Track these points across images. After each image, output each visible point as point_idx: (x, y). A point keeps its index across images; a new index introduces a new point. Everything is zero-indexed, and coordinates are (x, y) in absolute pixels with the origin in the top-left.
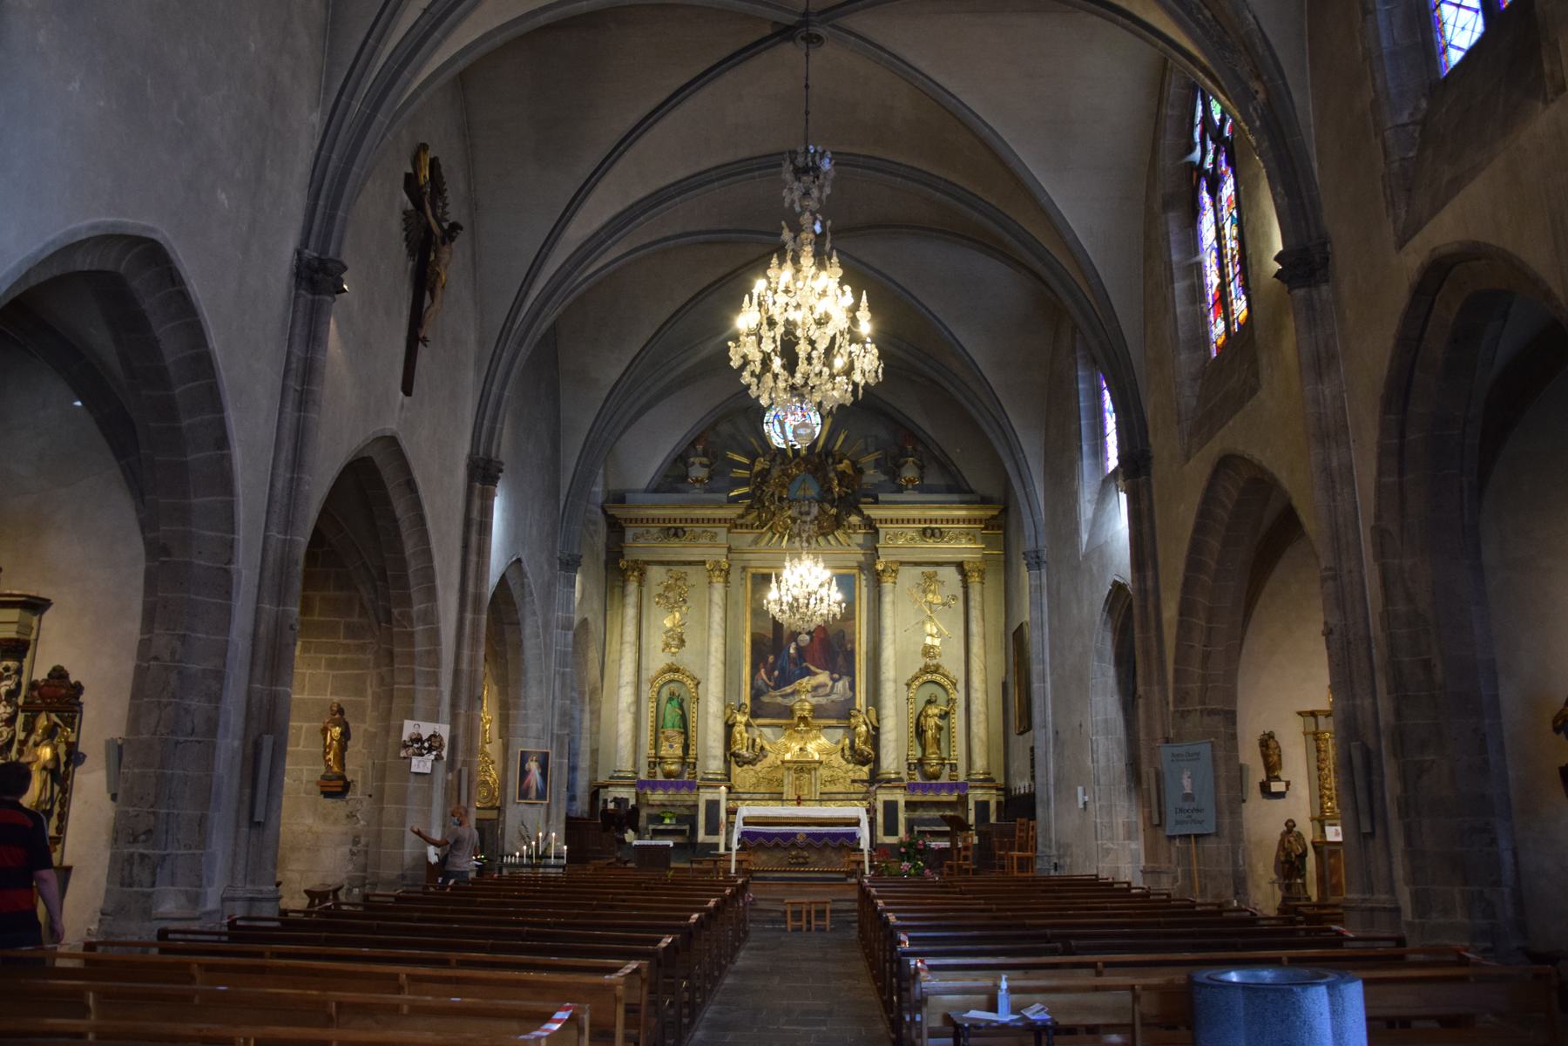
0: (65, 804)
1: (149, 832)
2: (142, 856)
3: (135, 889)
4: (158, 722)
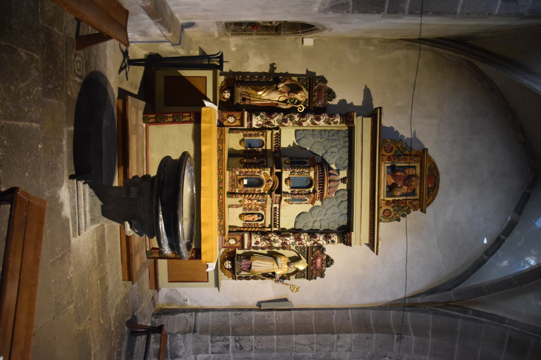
0: (255, 278)
1: (241, 348)
2: (227, 346)
3: (210, 344)
4: (302, 345)
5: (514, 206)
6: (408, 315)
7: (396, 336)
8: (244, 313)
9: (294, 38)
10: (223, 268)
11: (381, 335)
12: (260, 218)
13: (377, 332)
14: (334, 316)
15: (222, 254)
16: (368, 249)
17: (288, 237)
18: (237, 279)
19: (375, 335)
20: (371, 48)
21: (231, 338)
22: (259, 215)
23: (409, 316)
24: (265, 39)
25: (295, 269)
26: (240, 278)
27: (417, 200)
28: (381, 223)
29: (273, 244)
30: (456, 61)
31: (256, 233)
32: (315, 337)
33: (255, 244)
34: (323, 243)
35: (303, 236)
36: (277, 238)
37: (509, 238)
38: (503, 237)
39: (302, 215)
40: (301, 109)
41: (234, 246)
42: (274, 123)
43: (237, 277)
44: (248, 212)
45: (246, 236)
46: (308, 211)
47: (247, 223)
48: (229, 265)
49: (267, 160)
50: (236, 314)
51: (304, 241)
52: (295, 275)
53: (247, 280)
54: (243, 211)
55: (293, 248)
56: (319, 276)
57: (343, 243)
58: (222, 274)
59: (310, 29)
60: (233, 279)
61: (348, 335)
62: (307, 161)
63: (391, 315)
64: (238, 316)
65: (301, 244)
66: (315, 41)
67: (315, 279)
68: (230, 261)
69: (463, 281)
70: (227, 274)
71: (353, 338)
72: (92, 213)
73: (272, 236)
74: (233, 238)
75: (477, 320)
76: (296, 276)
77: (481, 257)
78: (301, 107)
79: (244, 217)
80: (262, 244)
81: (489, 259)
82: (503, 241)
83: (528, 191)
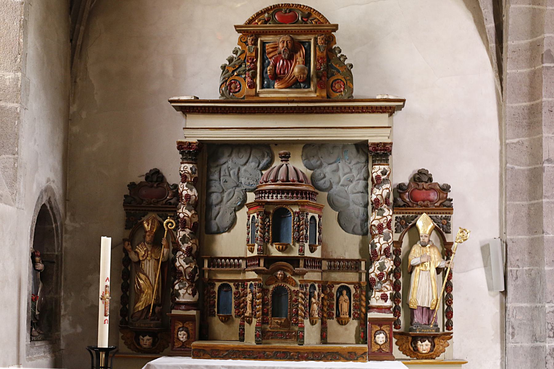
6: (513, 44)
7: (546, 65)
8: (511, 319)
10: (431, 355)
11: (544, 89)
12: (345, 292)
13: (540, 96)
14: (516, 167)
15: (407, 356)
16: (398, 115)
17: (376, 246)
18: (451, 331)
19: (544, 99)
20: (84, 115)
21: (550, 345)
22: (340, 291)
23: (516, 42)
24: (65, 279)
25: (434, 233)
26: (449, 325)
27: (316, 39)
29: (386, 270)
31: (368, 298)
32: (548, 200)
33: (386, 301)
34: (387, 189)
35: (374, 221)
36: (377, 264)
39: (342, 222)
40: (170, 224)
41: (388, 335)
44: (334, 312)
45: (371, 315)
47: (352, 312)
49: (249, 280)
50: (513, 335)
52: (444, 233)
53: (452, 315)
55: (396, 237)
56: (447, 194)
57: (388, 156)
58: (442, 355)
59: (50, 211)
61: (544, 144)
62: (251, 216)
63: (514, 71)
64: (516, 332)
68: (417, 342)
70: (441, 348)
71: (551, 135)
73: (373, 272)
74: (375, 337)
76: (447, 232)
78: (168, 223)
79: (341, 318)
80: (387, 289)
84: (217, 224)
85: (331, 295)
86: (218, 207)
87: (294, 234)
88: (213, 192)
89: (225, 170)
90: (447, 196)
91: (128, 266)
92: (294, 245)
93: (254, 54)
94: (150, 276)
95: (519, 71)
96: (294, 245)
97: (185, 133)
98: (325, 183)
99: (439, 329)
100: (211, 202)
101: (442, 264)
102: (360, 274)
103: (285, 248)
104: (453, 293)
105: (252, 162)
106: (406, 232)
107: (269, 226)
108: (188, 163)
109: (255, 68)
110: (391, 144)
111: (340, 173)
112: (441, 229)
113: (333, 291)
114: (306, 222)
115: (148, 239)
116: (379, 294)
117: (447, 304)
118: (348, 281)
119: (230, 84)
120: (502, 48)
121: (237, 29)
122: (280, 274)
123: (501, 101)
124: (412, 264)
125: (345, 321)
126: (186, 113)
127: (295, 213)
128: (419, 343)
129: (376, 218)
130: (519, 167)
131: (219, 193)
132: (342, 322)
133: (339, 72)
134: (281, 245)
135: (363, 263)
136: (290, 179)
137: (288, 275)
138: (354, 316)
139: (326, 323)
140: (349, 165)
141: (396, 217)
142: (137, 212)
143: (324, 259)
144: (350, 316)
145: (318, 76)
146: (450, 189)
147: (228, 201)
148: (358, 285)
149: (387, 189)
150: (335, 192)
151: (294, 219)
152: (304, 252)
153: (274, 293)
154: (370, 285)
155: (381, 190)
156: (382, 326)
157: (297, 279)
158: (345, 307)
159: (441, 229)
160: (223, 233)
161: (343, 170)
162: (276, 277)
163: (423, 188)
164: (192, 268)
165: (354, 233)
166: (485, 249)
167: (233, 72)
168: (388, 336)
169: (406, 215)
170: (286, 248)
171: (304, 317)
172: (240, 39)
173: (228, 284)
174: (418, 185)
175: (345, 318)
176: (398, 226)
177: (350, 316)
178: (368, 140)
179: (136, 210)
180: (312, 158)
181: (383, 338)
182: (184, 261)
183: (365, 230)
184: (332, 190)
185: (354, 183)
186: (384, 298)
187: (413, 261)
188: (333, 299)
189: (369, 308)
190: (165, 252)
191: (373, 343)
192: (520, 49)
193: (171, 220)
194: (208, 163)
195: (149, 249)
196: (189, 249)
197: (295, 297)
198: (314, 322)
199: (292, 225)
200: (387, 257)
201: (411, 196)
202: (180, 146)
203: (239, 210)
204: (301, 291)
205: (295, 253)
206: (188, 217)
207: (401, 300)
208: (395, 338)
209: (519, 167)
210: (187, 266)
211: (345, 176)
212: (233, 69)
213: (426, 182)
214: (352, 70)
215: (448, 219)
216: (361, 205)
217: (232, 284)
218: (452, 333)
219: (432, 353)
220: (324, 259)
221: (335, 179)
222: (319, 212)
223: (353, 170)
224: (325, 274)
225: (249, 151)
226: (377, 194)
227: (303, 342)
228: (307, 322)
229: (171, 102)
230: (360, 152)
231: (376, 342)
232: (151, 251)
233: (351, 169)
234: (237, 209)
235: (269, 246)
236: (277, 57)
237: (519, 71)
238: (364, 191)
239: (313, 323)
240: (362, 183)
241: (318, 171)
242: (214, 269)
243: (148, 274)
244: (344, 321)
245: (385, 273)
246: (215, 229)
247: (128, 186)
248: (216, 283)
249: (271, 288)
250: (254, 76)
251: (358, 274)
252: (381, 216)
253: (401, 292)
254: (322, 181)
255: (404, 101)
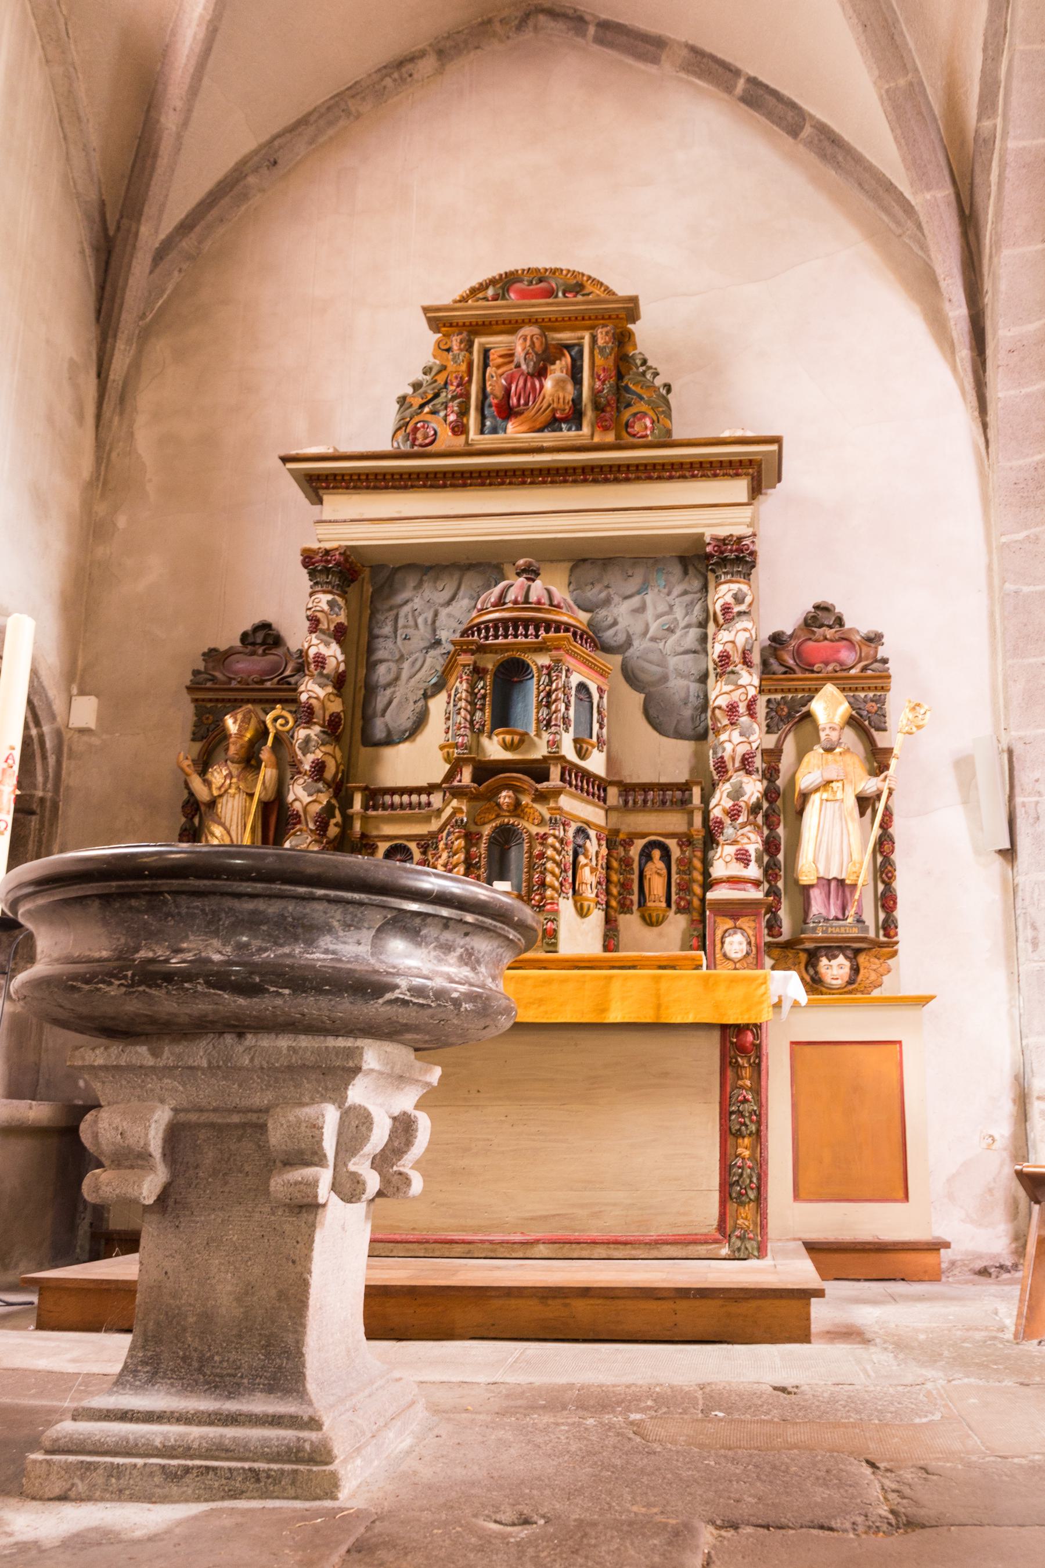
5: (641, 66)
6: (1009, 334)
9: (69, 758)
12: (656, 853)
14: (1026, 589)
17: (724, 750)
18: (895, 939)
20: (122, 521)
22: (646, 855)
23: (1015, 331)
26: (889, 926)
28: (677, 435)
29: (745, 798)
30: (180, 271)
31: (707, 863)
33: (747, 865)
34: (745, 630)
36: (725, 788)
37: (739, 65)
38: (741, 83)
39: (653, 712)
40: (280, 721)
42: (320, 803)
43: (885, 939)
44: (635, 898)
46: (643, 696)
47: (674, 897)
48: (834, 962)
51: (736, 696)
52: (873, 730)
53: (895, 903)
54: (632, 913)
56: (876, 648)
60: (895, 954)
63: (1012, 392)
65: (751, 706)
66: (82, 693)
67: (885, 661)
69: (890, 187)
70: (873, 976)
72: (239, 1385)
74: (723, 943)
75: (1005, 88)
76: (878, 729)
77: (809, 144)
78: (275, 720)
81: (812, 117)
82: (753, 81)
83: (592, 30)
84: (387, 725)
85: (626, 862)
86: (388, 692)
87: (538, 712)
88: (381, 661)
89: (406, 616)
90: (876, 652)
91: (193, 816)
92: (538, 735)
93: (464, 367)
94: (234, 827)
95: (1024, 391)
96: (538, 735)
97: (318, 532)
98: (615, 634)
99: (868, 927)
100: (375, 678)
101: (870, 785)
102: (691, 813)
103: (522, 741)
104: (897, 857)
105: (463, 598)
106: (789, 730)
107: (484, 697)
108: (324, 592)
109: (467, 395)
110: (754, 535)
111: (650, 613)
112: (867, 723)
113: (631, 853)
114: (566, 687)
115: (232, 750)
116: (730, 850)
117: (883, 882)
118: (664, 831)
119: (415, 430)
120: (984, 363)
121: (429, 315)
122: (505, 797)
123: (986, 467)
124: (803, 787)
125: (658, 915)
126: (321, 492)
127: (540, 669)
128: (824, 961)
129: (723, 691)
130: (1032, 588)
131: (393, 661)
132: (651, 921)
133: (641, 398)
134: (507, 733)
135: (696, 791)
136: (531, 600)
137: (526, 800)
138: (678, 904)
139: (616, 921)
140: (668, 598)
141: (769, 701)
142: (220, 705)
143: (612, 783)
144: (669, 905)
145: (598, 407)
146: (883, 640)
147: (411, 678)
148: (686, 840)
149: (745, 630)
150: (638, 654)
151: (539, 681)
152: (558, 747)
153: (493, 841)
154: (710, 839)
155: (733, 633)
156: (738, 919)
157: (542, 809)
158: (657, 886)
159: (867, 723)
160: (399, 743)
161: (655, 608)
162: (498, 805)
163: (826, 639)
164: (320, 803)
165: (679, 735)
166: (964, 766)
167: (422, 406)
168: (753, 942)
169: (790, 696)
170: (522, 741)
171: (560, 891)
172: (438, 344)
173: (405, 846)
174: (814, 633)
175: (657, 909)
176: (772, 718)
177: (669, 905)
178: (703, 535)
179: (217, 700)
180: (589, 587)
181: (740, 944)
182: (304, 789)
183: (701, 729)
184: (631, 650)
185: (679, 633)
186: (743, 858)
187: (804, 782)
188: (632, 869)
189: (709, 884)
190: (267, 778)
191: (718, 956)
192: (1025, 343)
193: (285, 713)
194: (371, 602)
195: (235, 772)
196: (319, 768)
197: (540, 848)
198: (585, 910)
199: (535, 692)
200: (749, 773)
201: (798, 654)
202: (309, 559)
203: (433, 695)
204: (552, 832)
205: (540, 751)
206: (317, 698)
207: (782, 873)
208: (769, 956)
209: (1032, 588)
210: (310, 799)
211: (660, 620)
212: (421, 401)
213: (830, 627)
214: (670, 396)
215: (880, 701)
216: (693, 678)
217: (413, 846)
218: (897, 943)
219: (853, 986)
220: (612, 783)
221: (637, 628)
222: (601, 681)
223: (675, 607)
224: (614, 816)
225: (456, 576)
226: (723, 641)
227: (555, 945)
228: (566, 907)
229: (285, 460)
230: (690, 572)
231: (725, 955)
232: (238, 776)
233: (671, 607)
234: (429, 693)
235: (485, 740)
236: (512, 374)
237: (1024, 391)
238: (699, 648)
239: (582, 912)
240: (694, 633)
241: (602, 613)
242: (374, 813)
243: (227, 824)
244: (654, 914)
245: (742, 804)
246: (380, 733)
247: (204, 654)
248: (379, 844)
249: (487, 830)
250: (464, 412)
251: (686, 817)
252: (733, 684)
253: (781, 857)
254: (611, 632)
255: (777, 440)
